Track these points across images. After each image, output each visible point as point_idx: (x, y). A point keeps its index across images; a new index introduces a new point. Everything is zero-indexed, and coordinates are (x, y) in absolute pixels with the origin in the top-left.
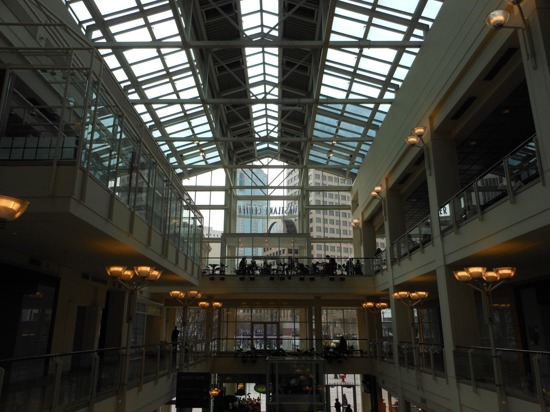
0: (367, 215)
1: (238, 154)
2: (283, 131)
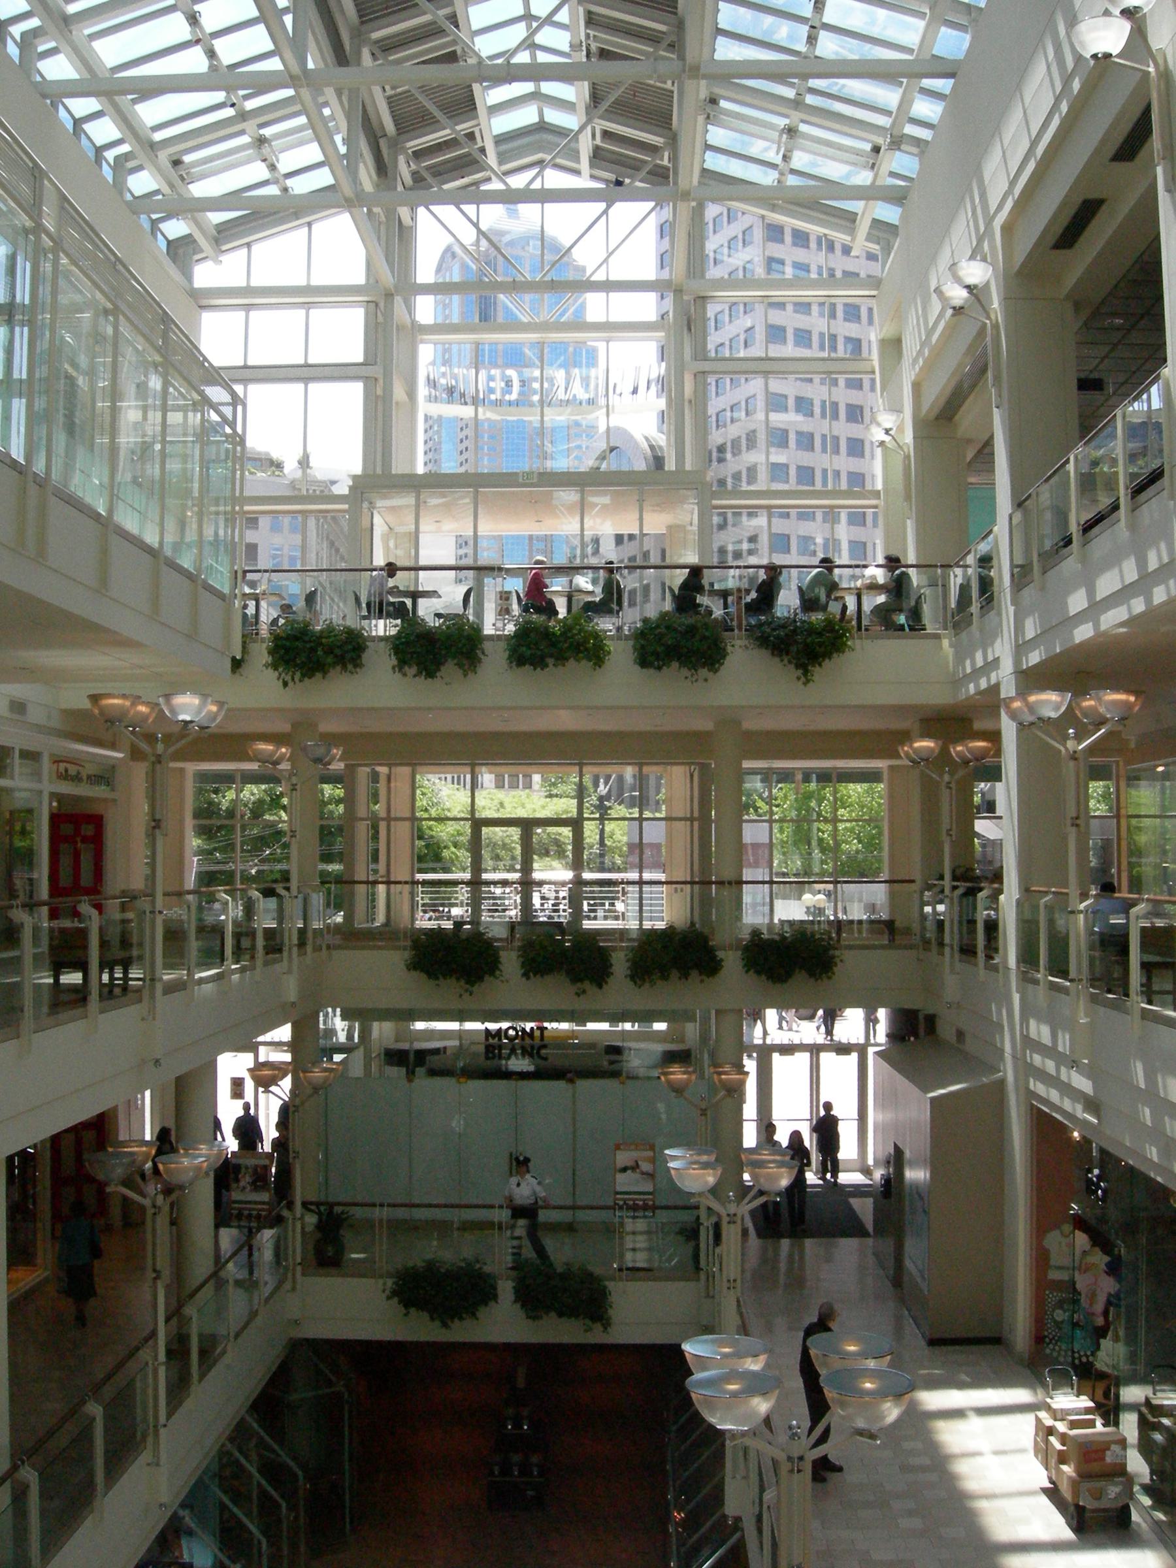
0: (935, 393)
1: (418, 155)
2: (594, 47)
